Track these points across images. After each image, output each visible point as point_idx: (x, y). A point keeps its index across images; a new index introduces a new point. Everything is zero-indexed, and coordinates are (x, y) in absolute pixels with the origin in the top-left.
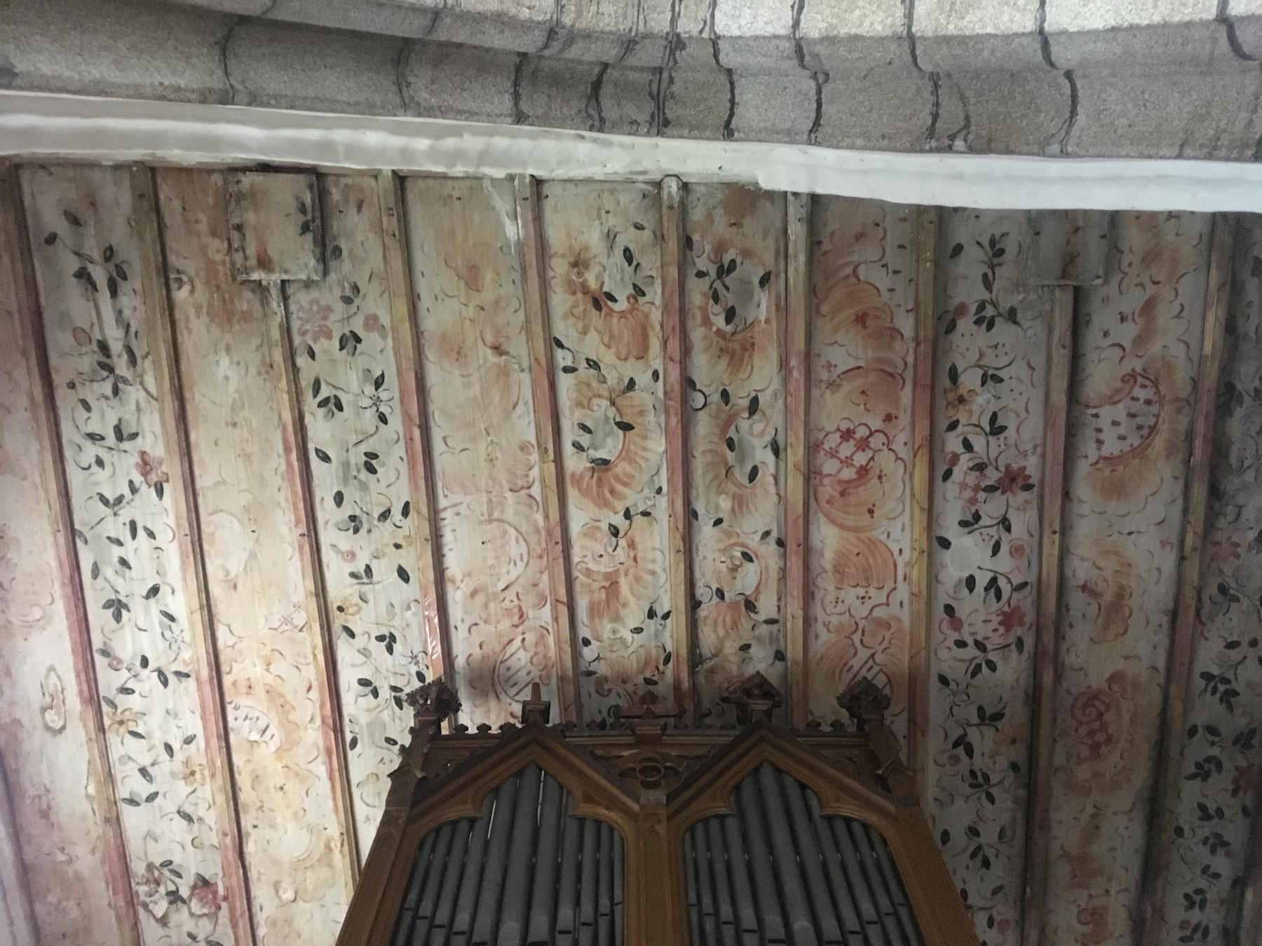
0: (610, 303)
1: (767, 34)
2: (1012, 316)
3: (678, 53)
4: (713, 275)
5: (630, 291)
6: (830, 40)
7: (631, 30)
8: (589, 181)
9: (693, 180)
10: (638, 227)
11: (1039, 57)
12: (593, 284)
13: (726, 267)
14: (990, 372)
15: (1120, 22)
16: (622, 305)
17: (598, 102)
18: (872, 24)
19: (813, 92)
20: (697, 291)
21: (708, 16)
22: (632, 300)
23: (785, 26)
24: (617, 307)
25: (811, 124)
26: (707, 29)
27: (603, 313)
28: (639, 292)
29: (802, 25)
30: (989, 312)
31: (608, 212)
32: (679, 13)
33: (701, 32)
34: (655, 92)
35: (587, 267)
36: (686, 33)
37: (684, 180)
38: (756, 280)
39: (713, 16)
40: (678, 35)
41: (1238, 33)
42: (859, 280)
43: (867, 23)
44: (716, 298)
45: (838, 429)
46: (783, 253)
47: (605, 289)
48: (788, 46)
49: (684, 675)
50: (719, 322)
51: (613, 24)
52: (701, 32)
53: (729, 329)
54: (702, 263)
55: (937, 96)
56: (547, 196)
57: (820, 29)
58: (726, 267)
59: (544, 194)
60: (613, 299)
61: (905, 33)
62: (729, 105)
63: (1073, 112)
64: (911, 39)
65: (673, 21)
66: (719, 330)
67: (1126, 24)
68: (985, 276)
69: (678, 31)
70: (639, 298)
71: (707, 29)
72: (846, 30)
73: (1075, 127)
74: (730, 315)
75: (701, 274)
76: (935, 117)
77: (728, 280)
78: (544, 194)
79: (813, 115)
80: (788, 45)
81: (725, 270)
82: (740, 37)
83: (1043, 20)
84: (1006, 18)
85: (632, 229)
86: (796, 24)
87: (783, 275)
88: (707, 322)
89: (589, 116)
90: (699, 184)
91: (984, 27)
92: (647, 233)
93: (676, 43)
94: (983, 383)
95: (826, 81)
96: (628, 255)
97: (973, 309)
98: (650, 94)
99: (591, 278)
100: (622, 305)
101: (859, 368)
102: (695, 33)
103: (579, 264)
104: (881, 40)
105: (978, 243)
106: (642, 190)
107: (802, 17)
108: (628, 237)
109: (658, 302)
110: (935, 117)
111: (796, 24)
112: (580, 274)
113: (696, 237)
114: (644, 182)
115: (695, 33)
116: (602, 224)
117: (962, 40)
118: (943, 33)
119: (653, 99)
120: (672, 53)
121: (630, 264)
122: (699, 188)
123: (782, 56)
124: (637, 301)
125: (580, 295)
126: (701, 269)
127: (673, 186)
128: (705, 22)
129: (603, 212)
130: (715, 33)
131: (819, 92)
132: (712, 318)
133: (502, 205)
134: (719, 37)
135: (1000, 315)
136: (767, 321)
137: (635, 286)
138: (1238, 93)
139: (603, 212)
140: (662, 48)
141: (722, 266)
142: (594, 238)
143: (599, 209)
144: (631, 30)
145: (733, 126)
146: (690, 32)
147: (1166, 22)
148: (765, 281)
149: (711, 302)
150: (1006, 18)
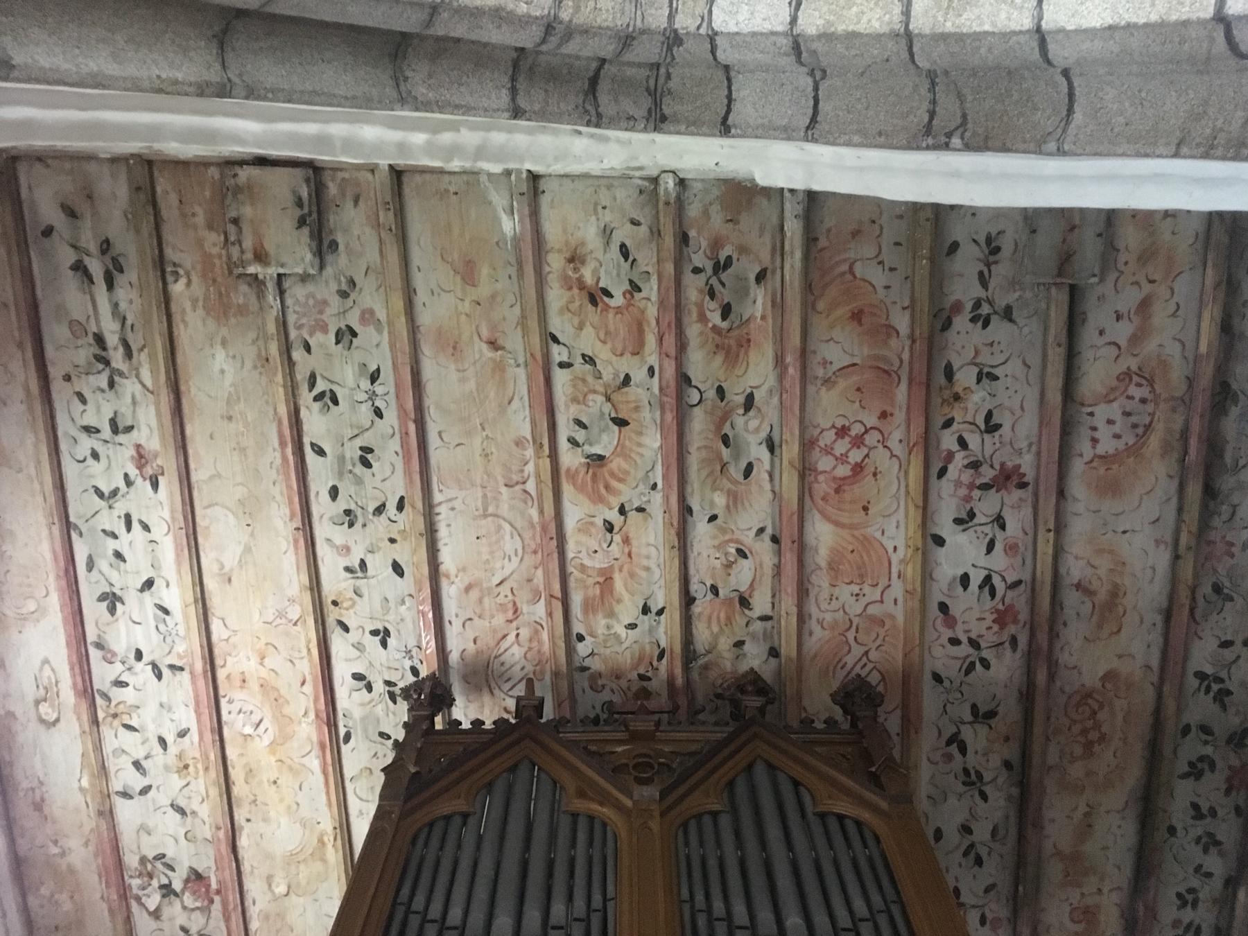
0: (606, 299)
1: (764, 31)
2: (1008, 314)
3: (675, 49)
4: (709, 271)
5: (627, 286)
6: (827, 37)
7: (628, 25)
8: (586, 176)
9: (689, 176)
10: (635, 223)
11: (1036, 55)
12: (589, 280)
13: (722, 263)
14: (986, 370)
15: (1118, 20)
16: (618, 300)
17: (595, 98)
18: (870, 21)
19: (810, 89)
20: (693, 287)
21: (706, 12)
22: (628, 296)
23: (782, 23)
24: (613, 303)
25: (808, 121)
26: (705, 25)
27: (599, 309)
28: (635, 287)
29: (800, 21)
30: (985, 309)
31: (604, 208)
32: (677, 9)
33: (699, 28)
34: (652, 88)
35: (583, 262)
36: (683, 29)
37: (681, 176)
38: (752, 277)
39: (710, 12)
40: (675, 31)
41: (1235, 32)
42: (855, 277)
43: (865, 19)
44: (712, 294)
45: (833, 426)
46: (779, 250)
47: (601, 285)
48: (785, 42)
49: (678, 671)
50: (715, 318)
51: (610, 19)
52: (699, 28)
53: (725, 325)
54: (699, 260)
55: (934, 94)
56: (544, 192)
57: (818, 26)
58: (722, 263)
59: (541, 189)
60: (609, 295)
61: (902, 30)
62: (726, 101)
63: (1070, 111)
64: (909, 37)
65: (671, 17)
66: (714, 326)
67: (1123, 23)
68: (981, 274)
69: (676, 26)
70: (635, 294)
71: (705, 25)
72: (844, 27)
73: (1072, 125)
74: (726, 311)
75: (697, 271)
76: (932, 114)
77: (724, 276)
78: (541, 189)
79: (810, 112)
80: (785, 41)
81: (721, 267)
82: (737, 33)
83: (1040, 18)
84: (1003, 15)
85: (629, 225)
86: (794, 21)
87: (779, 271)
88: (703, 318)
89: (586, 111)
90: (695, 180)
91: (981, 24)
92: (644, 229)
93: (673, 39)
94: (979, 381)
95: (823, 78)
96: (624, 251)
97: (969, 306)
98: (648, 90)
99: (587, 274)
100: (618, 300)
101: (854, 365)
102: (692, 29)
103: (575, 259)
104: (878, 37)
105: (974, 241)
106: (638, 186)
107: (800, 13)
108: (623, 233)
109: (654, 298)
110: (932, 114)
111: (794, 21)
112: (576, 270)
113: (692, 233)
114: (641, 178)
115: (692, 29)
116: (598, 219)
117: (960, 38)
118: (940, 31)
119: (650, 94)
120: (670, 49)
121: (626, 259)
122: (698, 186)
123: (779, 53)
124: (633, 297)
125: (576, 291)
126: (697, 265)
127: (670, 182)
128: (703, 19)
129: (600, 208)
130: (713, 29)
131: (816, 89)
132: (708, 314)
133: (499, 200)
134: (716, 34)
135: (996, 313)
136: (763, 318)
137: (631, 281)
138: (1235, 92)
139: (600, 208)
140: (659, 44)
141: (718, 262)
142: (590, 234)
143: (596, 204)
144: (628, 25)
145: (730, 122)
146: (687, 28)
147: (1163, 21)
148: (761, 277)
149: (707, 298)
150: (1003, 15)
